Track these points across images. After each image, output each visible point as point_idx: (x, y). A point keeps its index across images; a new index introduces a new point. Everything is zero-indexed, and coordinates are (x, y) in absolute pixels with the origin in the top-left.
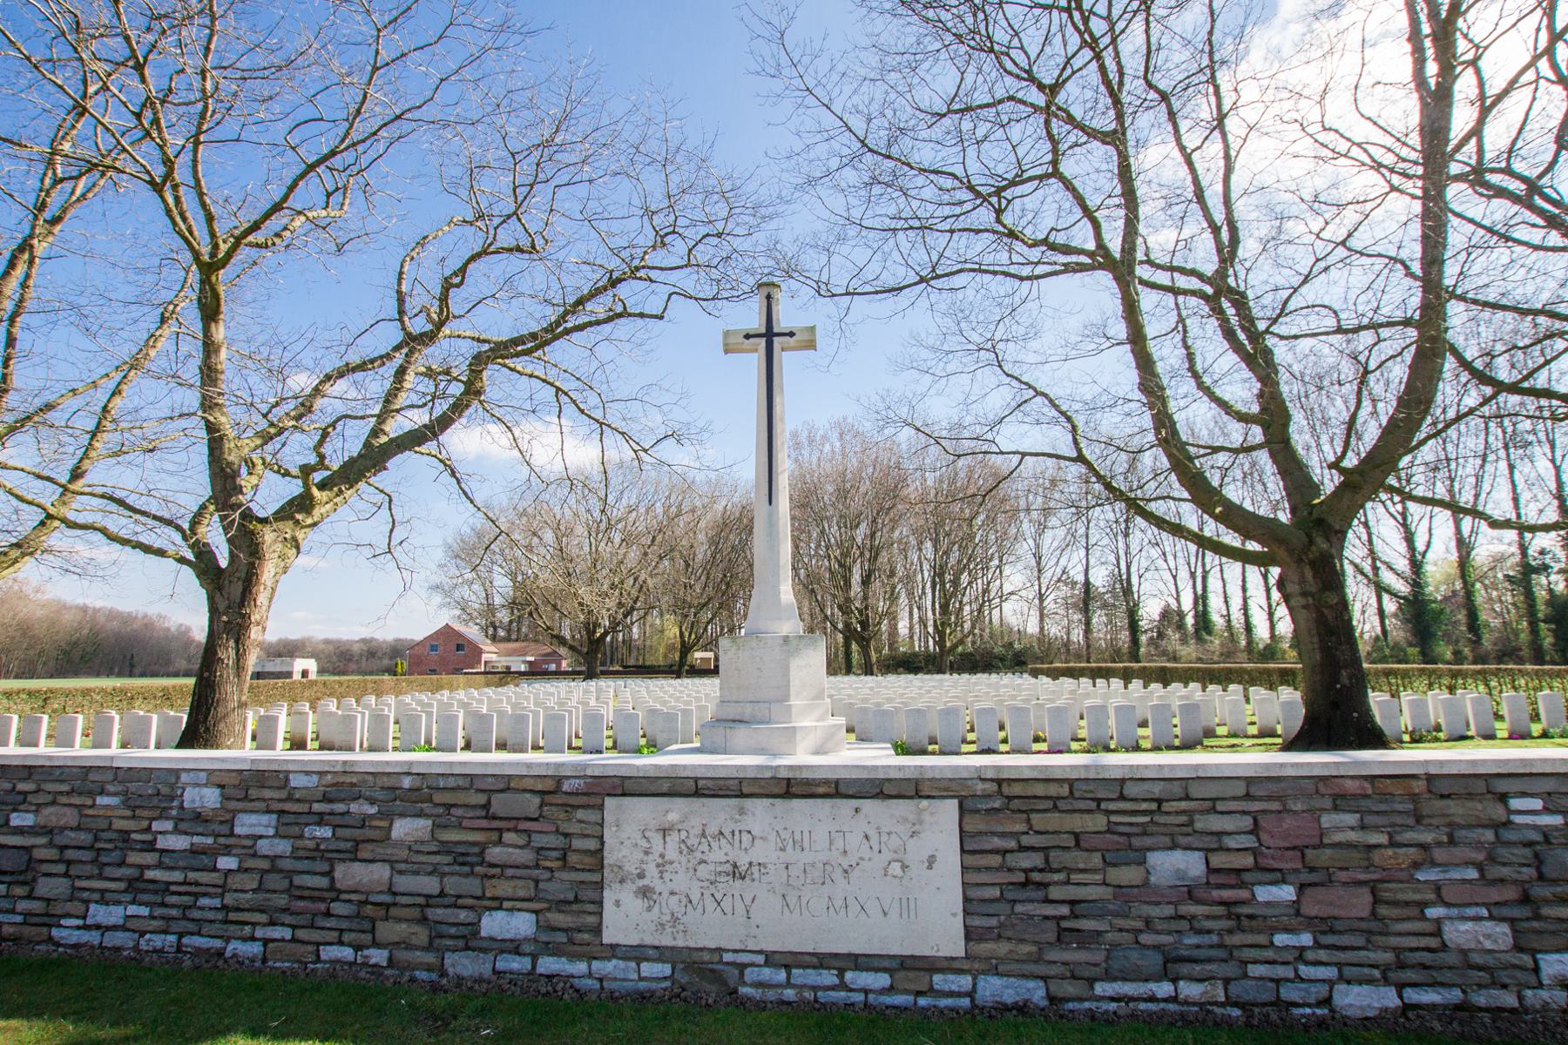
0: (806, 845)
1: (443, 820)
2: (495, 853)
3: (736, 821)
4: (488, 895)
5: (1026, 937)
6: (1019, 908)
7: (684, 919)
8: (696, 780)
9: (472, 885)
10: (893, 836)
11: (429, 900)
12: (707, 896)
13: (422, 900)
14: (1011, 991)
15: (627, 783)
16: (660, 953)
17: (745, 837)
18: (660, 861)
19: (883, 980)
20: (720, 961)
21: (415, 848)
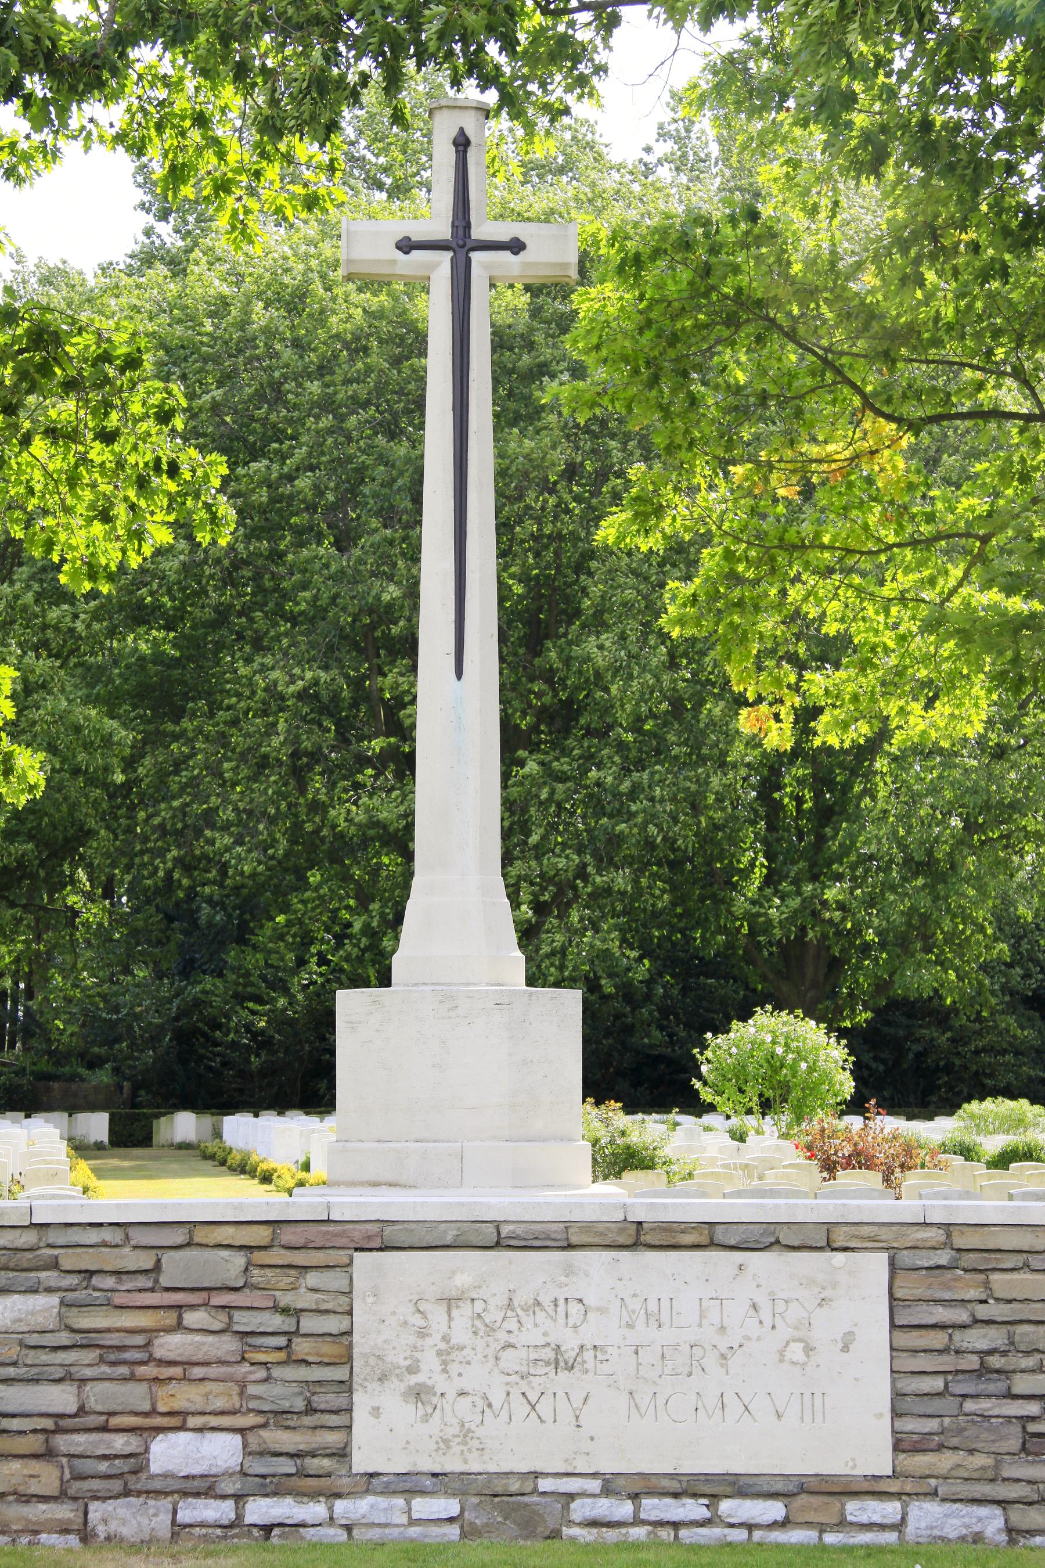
0: (665, 1317)
1: (81, 1295)
2: (170, 1345)
4: (162, 1408)
6: (970, 1406)
7: (480, 1432)
8: (497, 1224)
9: (136, 1395)
10: (794, 1305)
11: (60, 1423)
13: (48, 1424)
14: (956, 1522)
15: (388, 1230)
16: (440, 1481)
17: (574, 1308)
18: (443, 1346)
19: (775, 1510)
20: (535, 1491)
21: (34, 1340)
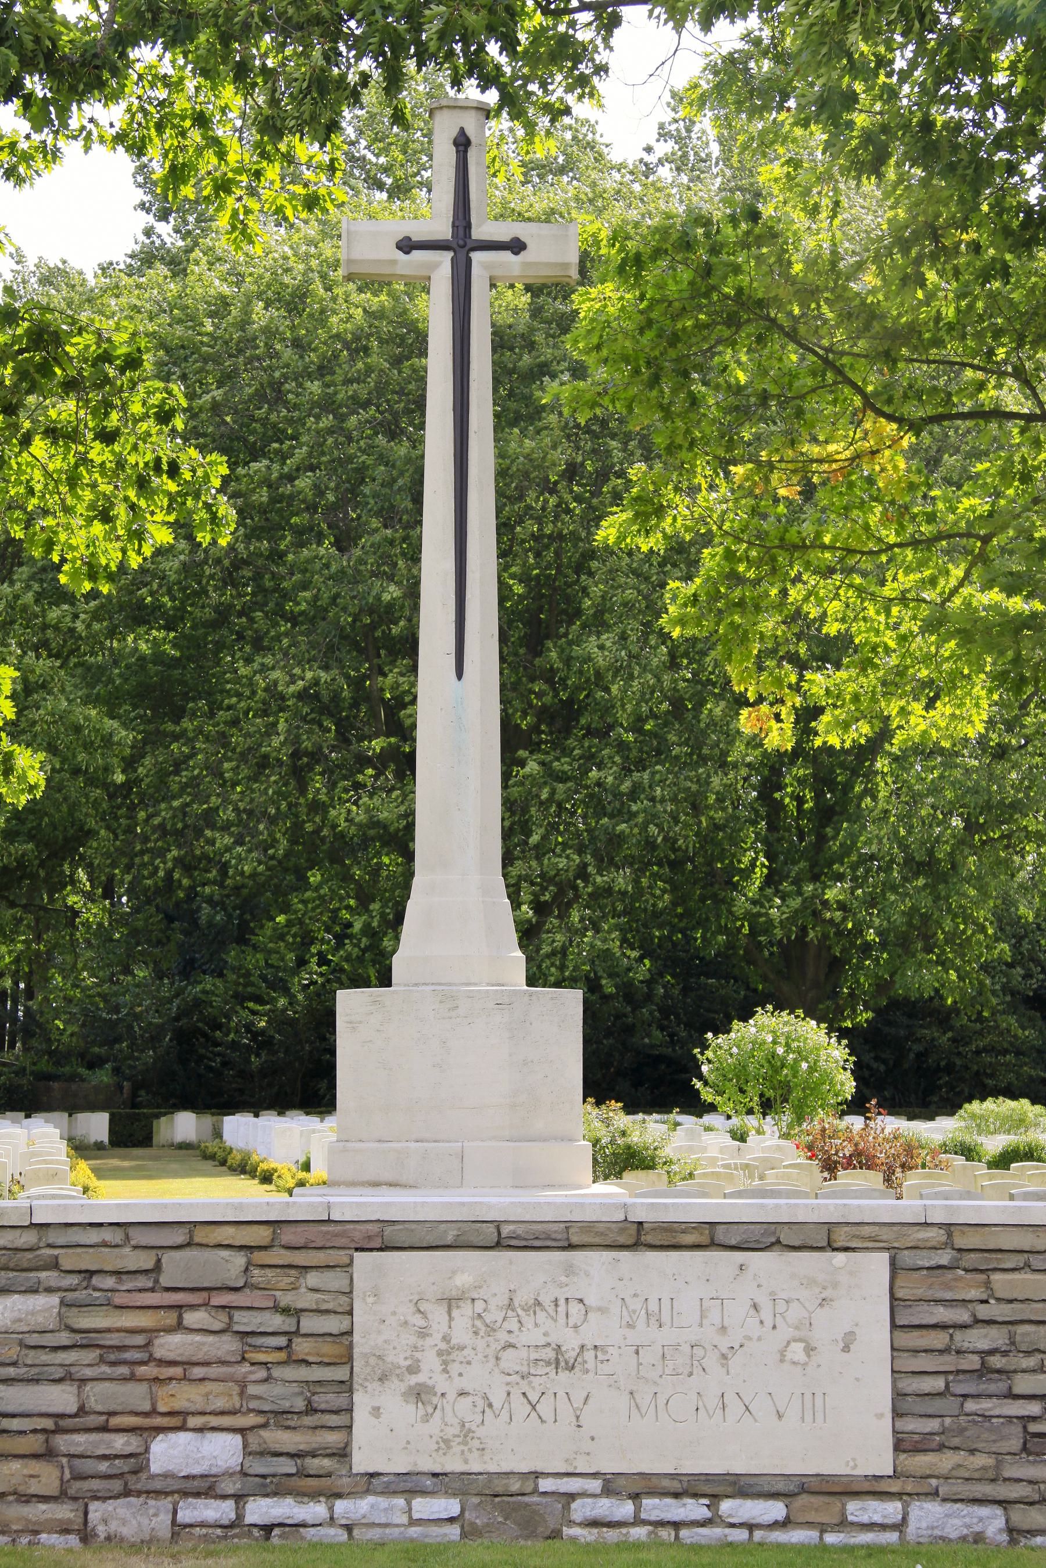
0: (666, 1318)
1: (81, 1295)
2: (171, 1345)
3: (561, 1286)
4: (162, 1408)
5: (980, 1446)
6: (971, 1406)
7: (480, 1432)
8: (498, 1224)
9: (136, 1395)
10: (794, 1305)
11: (61, 1423)
12: (516, 1394)
13: (48, 1424)
14: (957, 1522)
16: (441, 1482)
17: (575, 1308)
18: (443, 1346)
19: (776, 1510)
20: (535, 1491)
21: (34, 1340)
